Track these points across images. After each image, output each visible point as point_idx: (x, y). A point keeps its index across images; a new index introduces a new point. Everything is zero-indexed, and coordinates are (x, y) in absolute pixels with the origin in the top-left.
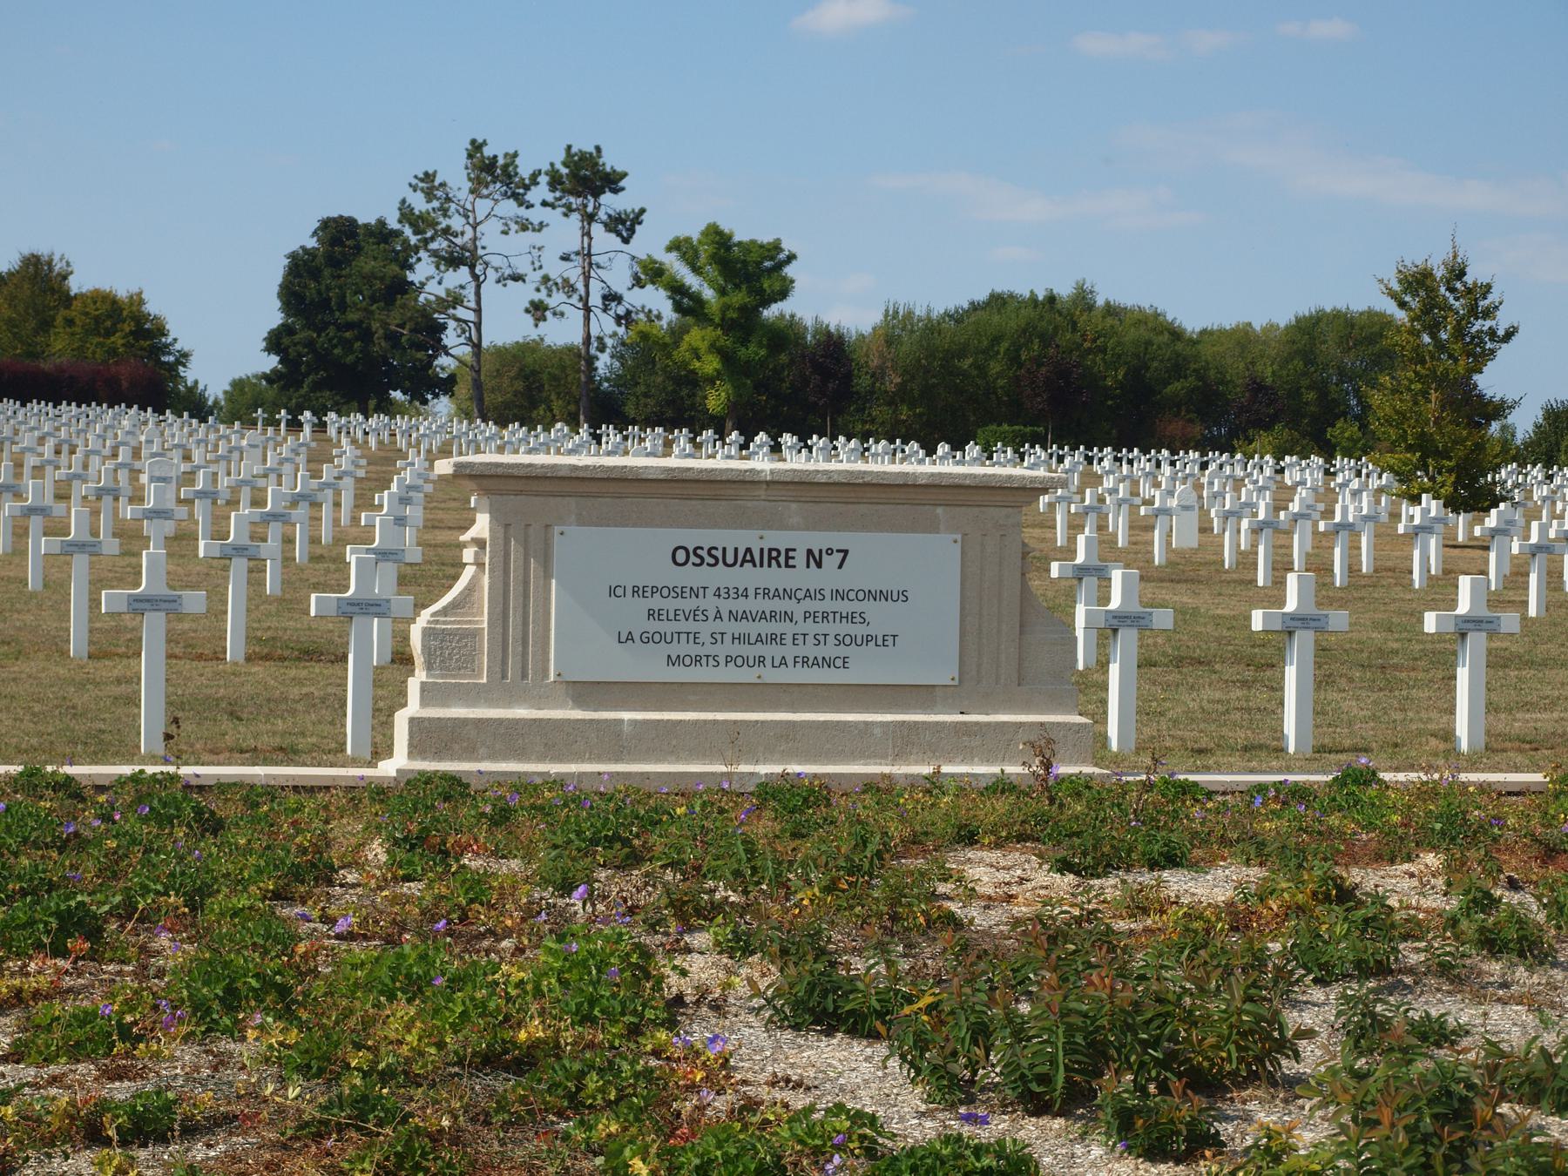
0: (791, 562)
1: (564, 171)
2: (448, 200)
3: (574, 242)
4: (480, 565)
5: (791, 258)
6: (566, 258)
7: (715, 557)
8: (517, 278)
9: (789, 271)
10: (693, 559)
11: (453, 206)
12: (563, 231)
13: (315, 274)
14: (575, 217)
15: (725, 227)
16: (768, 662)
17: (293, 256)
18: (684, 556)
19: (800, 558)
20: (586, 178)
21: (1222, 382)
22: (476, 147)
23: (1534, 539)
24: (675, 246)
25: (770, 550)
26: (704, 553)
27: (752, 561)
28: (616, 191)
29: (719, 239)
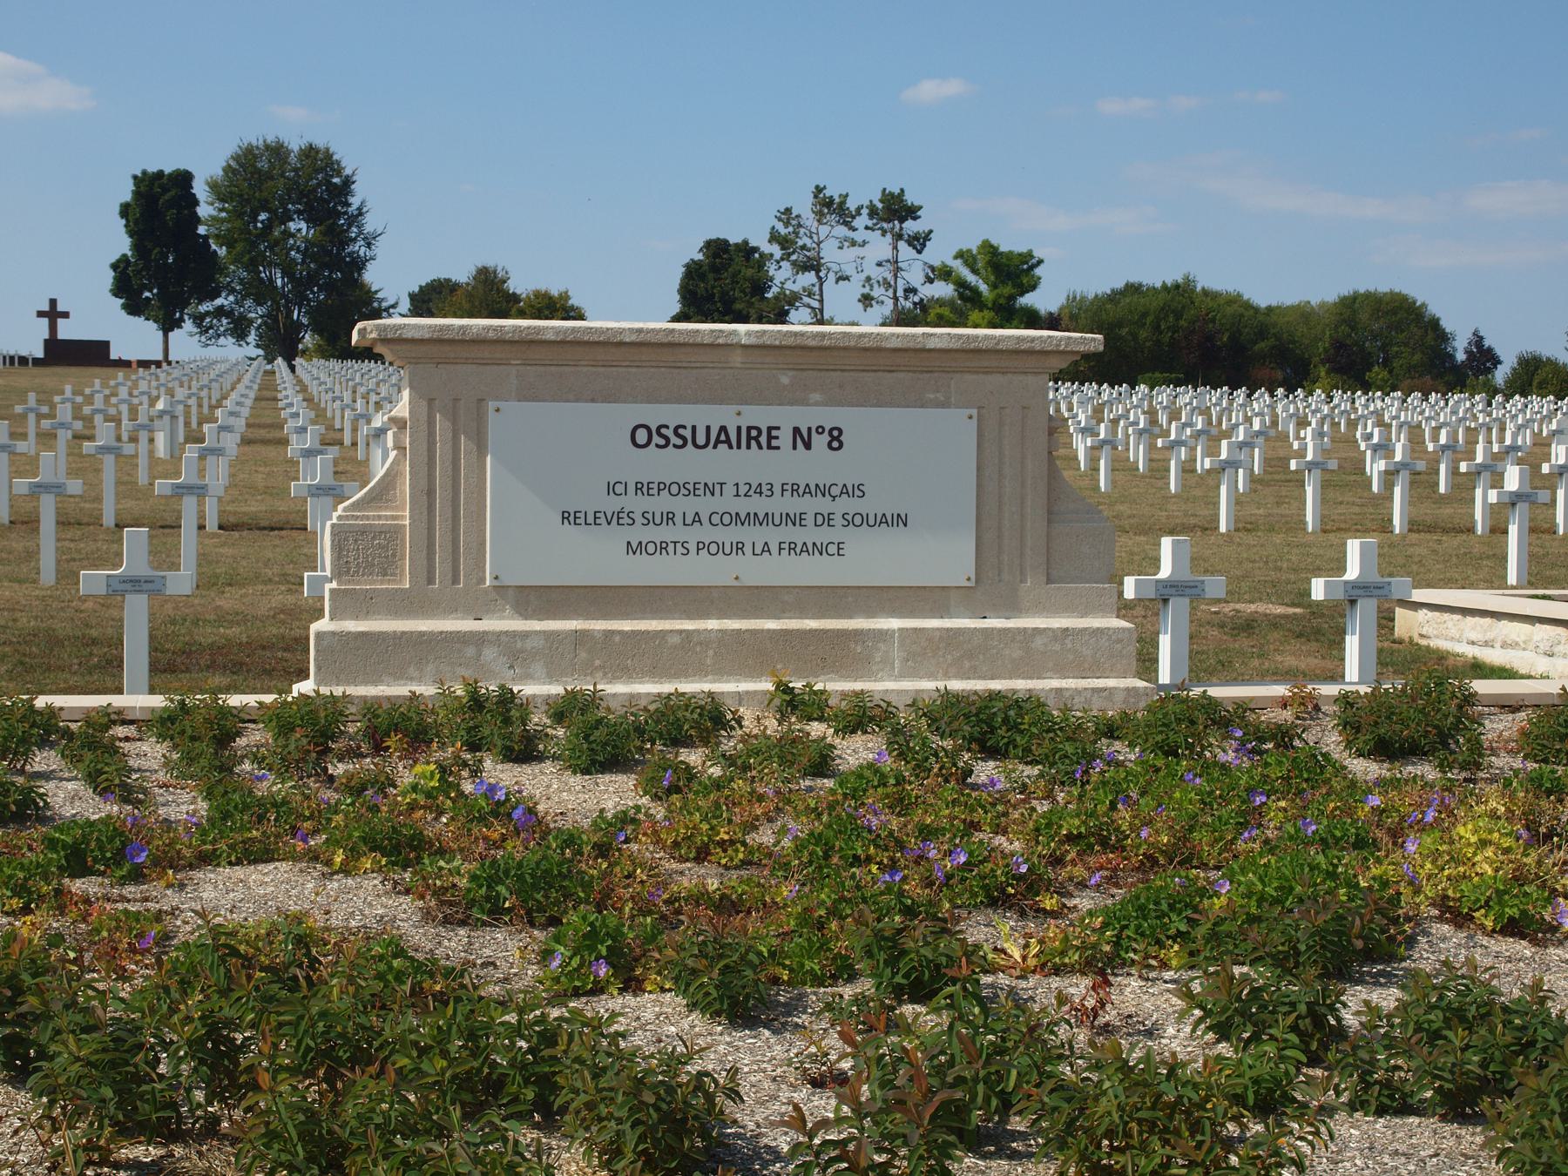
0: (774, 443)
1: (880, 206)
2: (800, 226)
3: (887, 253)
4: (399, 447)
5: (1040, 262)
6: (879, 264)
7: (683, 438)
8: (847, 278)
9: (1038, 271)
10: (656, 439)
11: (802, 231)
12: (880, 246)
13: (702, 277)
14: (889, 236)
15: (994, 242)
16: (748, 549)
17: (687, 266)
18: (646, 437)
19: (785, 438)
20: (895, 210)
21: (1294, 342)
22: (819, 190)
23: (1508, 442)
24: (960, 255)
25: (749, 429)
26: (669, 433)
27: (728, 442)
28: (915, 218)
29: (989, 249)
